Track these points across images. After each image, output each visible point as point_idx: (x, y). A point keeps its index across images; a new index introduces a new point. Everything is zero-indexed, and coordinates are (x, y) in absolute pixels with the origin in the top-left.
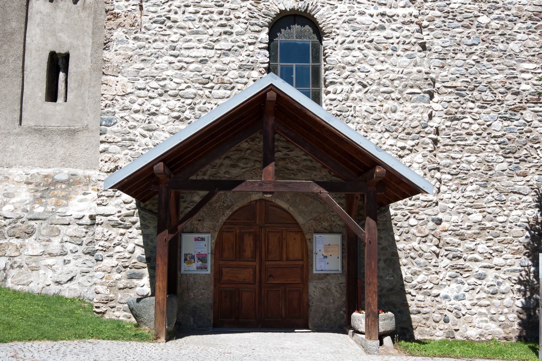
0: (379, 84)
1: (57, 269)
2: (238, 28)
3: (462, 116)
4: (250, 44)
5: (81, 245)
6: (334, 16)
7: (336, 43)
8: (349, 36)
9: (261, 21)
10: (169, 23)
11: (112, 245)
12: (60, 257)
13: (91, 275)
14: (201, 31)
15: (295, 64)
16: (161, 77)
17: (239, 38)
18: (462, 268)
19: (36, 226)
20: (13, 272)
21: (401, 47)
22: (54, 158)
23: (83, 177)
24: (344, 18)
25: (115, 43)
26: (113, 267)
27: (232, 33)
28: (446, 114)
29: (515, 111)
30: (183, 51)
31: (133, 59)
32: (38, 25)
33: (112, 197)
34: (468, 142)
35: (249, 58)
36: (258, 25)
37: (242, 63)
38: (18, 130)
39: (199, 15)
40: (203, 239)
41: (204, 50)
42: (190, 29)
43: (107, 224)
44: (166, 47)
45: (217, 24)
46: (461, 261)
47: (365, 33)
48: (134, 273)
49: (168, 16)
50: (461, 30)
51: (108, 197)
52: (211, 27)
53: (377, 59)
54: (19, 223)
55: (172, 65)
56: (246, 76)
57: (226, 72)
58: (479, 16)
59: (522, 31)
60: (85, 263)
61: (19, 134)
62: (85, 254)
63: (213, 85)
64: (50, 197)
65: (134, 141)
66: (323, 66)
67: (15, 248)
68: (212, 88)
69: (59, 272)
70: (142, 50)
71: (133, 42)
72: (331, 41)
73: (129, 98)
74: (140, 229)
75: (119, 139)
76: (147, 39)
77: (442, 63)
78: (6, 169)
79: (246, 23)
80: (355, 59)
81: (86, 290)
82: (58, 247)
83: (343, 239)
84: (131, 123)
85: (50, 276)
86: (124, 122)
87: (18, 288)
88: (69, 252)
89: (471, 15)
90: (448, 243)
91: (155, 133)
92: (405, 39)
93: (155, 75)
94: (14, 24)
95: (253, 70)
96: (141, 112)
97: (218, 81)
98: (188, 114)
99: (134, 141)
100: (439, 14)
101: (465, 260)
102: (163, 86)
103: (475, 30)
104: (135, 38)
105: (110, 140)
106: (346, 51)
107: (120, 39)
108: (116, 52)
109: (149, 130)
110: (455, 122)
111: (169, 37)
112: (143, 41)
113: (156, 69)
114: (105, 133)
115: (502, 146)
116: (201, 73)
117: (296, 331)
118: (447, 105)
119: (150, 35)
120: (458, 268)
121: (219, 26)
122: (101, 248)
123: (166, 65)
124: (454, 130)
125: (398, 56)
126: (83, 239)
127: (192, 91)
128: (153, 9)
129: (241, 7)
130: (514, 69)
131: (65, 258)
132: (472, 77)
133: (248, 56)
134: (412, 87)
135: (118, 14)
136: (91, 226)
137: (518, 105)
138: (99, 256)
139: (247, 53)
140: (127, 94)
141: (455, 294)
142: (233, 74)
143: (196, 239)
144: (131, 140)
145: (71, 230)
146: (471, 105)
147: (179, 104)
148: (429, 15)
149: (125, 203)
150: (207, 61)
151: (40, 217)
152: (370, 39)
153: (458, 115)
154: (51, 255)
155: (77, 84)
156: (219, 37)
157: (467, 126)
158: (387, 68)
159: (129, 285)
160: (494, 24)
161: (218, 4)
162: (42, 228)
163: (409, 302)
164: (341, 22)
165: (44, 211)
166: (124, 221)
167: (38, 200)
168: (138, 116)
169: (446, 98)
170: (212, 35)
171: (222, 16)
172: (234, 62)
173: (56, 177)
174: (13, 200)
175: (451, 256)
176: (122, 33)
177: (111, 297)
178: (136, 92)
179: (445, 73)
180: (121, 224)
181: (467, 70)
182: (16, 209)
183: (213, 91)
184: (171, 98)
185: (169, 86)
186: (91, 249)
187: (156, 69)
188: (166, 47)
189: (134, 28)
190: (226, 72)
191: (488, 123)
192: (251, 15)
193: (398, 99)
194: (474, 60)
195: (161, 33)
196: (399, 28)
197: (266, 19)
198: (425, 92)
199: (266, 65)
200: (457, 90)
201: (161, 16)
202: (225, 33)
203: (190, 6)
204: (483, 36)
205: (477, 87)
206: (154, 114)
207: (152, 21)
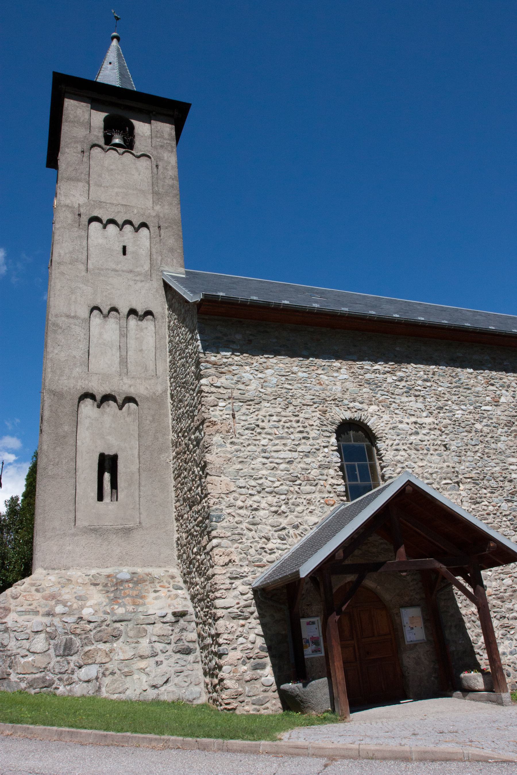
0: (423, 477)
1: (150, 671)
2: (312, 434)
3: (481, 500)
4: (324, 447)
5: (169, 644)
6: (382, 424)
7: (387, 445)
8: (395, 440)
9: (329, 428)
10: (259, 430)
11: (235, 637)
12: (151, 658)
13: (186, 674)
14: (285, 437)
15: (356, 463)
16: (258, 477)
17: (314, 442)
18: (509, 627)
19: (122, 628)
20: (107, 680)
21: (432, 448)
22: (111, 558)
23: (145, 576)
24: (390, 426)
25: (215, 447)
26: (239, 659)
27: (309, 438)
28: (470, 499)
29: (513, 494)
30: (273, 454)
31: (232, 461)
32: (88, 429)
33: (230, 589)
34: (489, 521)
35: (325, 458)
36: (329, 432)
37: (321, 463)
38: (73, 531)
39: (282, 423)
40: (313, 623)
41: (289, 452)
42: (276, 434)
43: (228, 616)
44: (259, 450)
45: (297, 431)
46: (506, 621)
47: (406, 437)
48: (258, 664)
49: (257, 424)
50: (466, 434)
51: (226, 590)
52: (292, 433)
53: (418, 457)
54: (104, 627)
55: (266, 466)
56: (325, 474)
57: (309, 471)
58: (475, 424)
59: (503, 434)
60: (177, 663)
61: (74, 535)
62: (176, 653)
63: (301, 482)
64: (124, 597)
65: (242, 535)
66: (378, 464)
67: (104, 654)
68: (300, 485)
69: (153, 675)
70: (238, 453)
71: (230, 446)
72: (383, 444)
73: (233, 496)
74: (258, 618)
75: (229, 534)
76: (242, 443)
77: (459, 460)
78: (63, 571)
79: (318, 430)
80: (402, 458)
81: (184, 691)
82: (149, 648)
83: (422, 611)
84: (237, 519)
85: (145, 680)
86: (232, 518)
87: (115, 697)
88: (160, 652)
89: (470, 423)
90: (494, 606)
91: (259, 527)
92: (433, 442)
93: (252, 475)
94: (66, 428)
95: (330, 468)
96: (244, 508)
97: (304, 479)
98: (283, 508)
99: (242, 535)
100: (450, 422)
101: (508, 619)
102: (260, 485)
103: (474, 434)
104: (232, 443)
105: (221, 535)
106: (395, 452)
107: (219, 444)
108: (217, 455)
109: (254, 524)
110: (478, 505)
111: (260, 442)
112: (239, 445)
113: (253, 469)
114: (216, 529)
115: (512, 523)
116: (290, 472)
117: (401, 702)
118: (469, 492)
119: (244, 440)
120: (506, 627)
121: (298, 432)
122: (225, 641)
123: (261, 466)
124: (478, 512)
125: (432, 454)
126: (171, 637)
127: (284, 487)
128: (243, 418)
129: (312, 417)
130: (505, 463)
131: (156, 658)
132: (480, 469)
133: (324, 457)
134: (445, 479)
135: (215, 422)
136: (176, 624)
137: (514, 490)
138: (225, 650)
139: (324, 454)
140: (231, 492)
141: (509, 649)
142: (315, 473)
143: (308, 624)
144: (239, 534)
145: (157, 629)
146: (485, 491)
147: (276, 500)
148: (444, 423)
149: (242, 594)
150: (293, 461)
151: (125, 618)
152: (410, 442)
153: (478, 500)
154: (142, 657)
155: (127, 483)
156: (299, 442)
157: (486, 508)
158: (426, 465)
159: (254, 677)
160: (486, 429)
161: (295, 414)
162: (128, 629)
163: (480, 662)
164: (387, 429)
165: (126, 612)
166: (243, 612)
167: (115, 600)
168: (242, 512)
169: (468, 486)
170: (294, 440)
171: (299, 424)
172: (314, 462)
173: (119, 576)
174: (89, 603)
175: (498, 617)
176: (220, 439)
177: (240, 691)
178: (238, 490)
179: (463, 467)
180: (240, 615)
181: (476, 464)
182: (96, 611)
183: (302, 488)
184: (268, 495)
185: (266, 484)
186: (181, 647)
187: (253, 469)
188: (258, 450)
189: (230, 434)
190: (309, 471)
191: (499, 505)
192: (321, 423)
193: (438, 489)
194: (479, 457)
195: (253, 438)
196: (428, 433)
197: (333, 427)
198: (455, 483)
199: (339, 464)
200: (473, 480)
201: (251, 424)
202: (304, 438)
203: (273, 416)
204: (481, 438)
205: (485, 477)
206: (256, 509)
207: (244, 428)
